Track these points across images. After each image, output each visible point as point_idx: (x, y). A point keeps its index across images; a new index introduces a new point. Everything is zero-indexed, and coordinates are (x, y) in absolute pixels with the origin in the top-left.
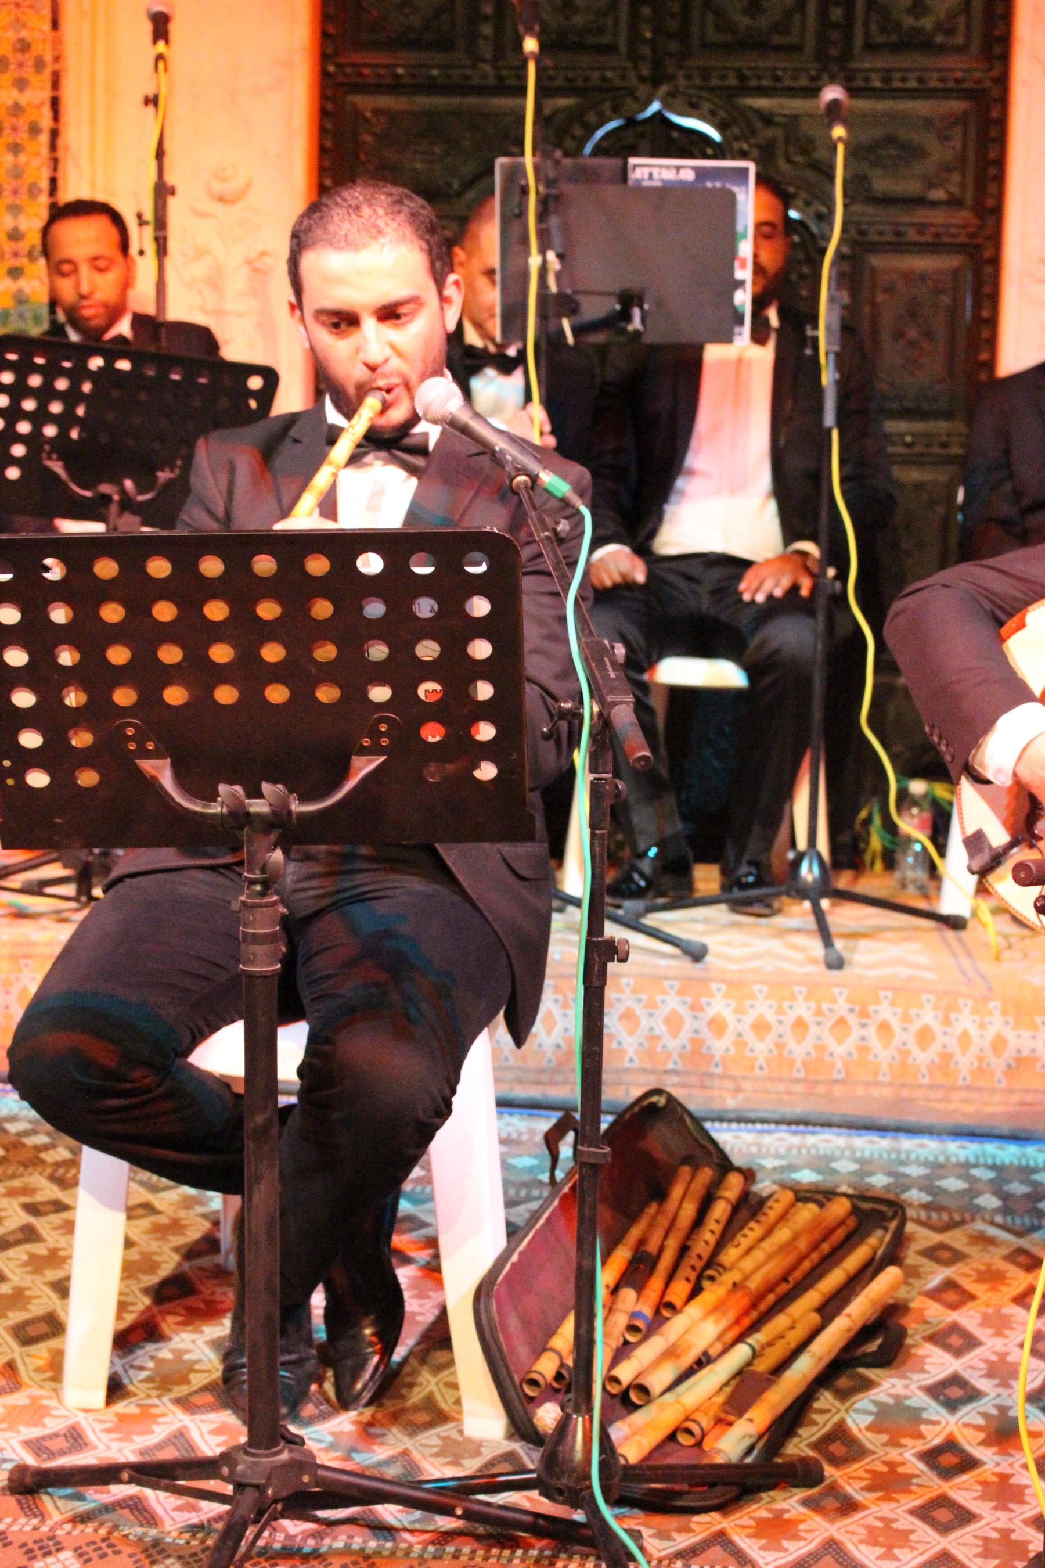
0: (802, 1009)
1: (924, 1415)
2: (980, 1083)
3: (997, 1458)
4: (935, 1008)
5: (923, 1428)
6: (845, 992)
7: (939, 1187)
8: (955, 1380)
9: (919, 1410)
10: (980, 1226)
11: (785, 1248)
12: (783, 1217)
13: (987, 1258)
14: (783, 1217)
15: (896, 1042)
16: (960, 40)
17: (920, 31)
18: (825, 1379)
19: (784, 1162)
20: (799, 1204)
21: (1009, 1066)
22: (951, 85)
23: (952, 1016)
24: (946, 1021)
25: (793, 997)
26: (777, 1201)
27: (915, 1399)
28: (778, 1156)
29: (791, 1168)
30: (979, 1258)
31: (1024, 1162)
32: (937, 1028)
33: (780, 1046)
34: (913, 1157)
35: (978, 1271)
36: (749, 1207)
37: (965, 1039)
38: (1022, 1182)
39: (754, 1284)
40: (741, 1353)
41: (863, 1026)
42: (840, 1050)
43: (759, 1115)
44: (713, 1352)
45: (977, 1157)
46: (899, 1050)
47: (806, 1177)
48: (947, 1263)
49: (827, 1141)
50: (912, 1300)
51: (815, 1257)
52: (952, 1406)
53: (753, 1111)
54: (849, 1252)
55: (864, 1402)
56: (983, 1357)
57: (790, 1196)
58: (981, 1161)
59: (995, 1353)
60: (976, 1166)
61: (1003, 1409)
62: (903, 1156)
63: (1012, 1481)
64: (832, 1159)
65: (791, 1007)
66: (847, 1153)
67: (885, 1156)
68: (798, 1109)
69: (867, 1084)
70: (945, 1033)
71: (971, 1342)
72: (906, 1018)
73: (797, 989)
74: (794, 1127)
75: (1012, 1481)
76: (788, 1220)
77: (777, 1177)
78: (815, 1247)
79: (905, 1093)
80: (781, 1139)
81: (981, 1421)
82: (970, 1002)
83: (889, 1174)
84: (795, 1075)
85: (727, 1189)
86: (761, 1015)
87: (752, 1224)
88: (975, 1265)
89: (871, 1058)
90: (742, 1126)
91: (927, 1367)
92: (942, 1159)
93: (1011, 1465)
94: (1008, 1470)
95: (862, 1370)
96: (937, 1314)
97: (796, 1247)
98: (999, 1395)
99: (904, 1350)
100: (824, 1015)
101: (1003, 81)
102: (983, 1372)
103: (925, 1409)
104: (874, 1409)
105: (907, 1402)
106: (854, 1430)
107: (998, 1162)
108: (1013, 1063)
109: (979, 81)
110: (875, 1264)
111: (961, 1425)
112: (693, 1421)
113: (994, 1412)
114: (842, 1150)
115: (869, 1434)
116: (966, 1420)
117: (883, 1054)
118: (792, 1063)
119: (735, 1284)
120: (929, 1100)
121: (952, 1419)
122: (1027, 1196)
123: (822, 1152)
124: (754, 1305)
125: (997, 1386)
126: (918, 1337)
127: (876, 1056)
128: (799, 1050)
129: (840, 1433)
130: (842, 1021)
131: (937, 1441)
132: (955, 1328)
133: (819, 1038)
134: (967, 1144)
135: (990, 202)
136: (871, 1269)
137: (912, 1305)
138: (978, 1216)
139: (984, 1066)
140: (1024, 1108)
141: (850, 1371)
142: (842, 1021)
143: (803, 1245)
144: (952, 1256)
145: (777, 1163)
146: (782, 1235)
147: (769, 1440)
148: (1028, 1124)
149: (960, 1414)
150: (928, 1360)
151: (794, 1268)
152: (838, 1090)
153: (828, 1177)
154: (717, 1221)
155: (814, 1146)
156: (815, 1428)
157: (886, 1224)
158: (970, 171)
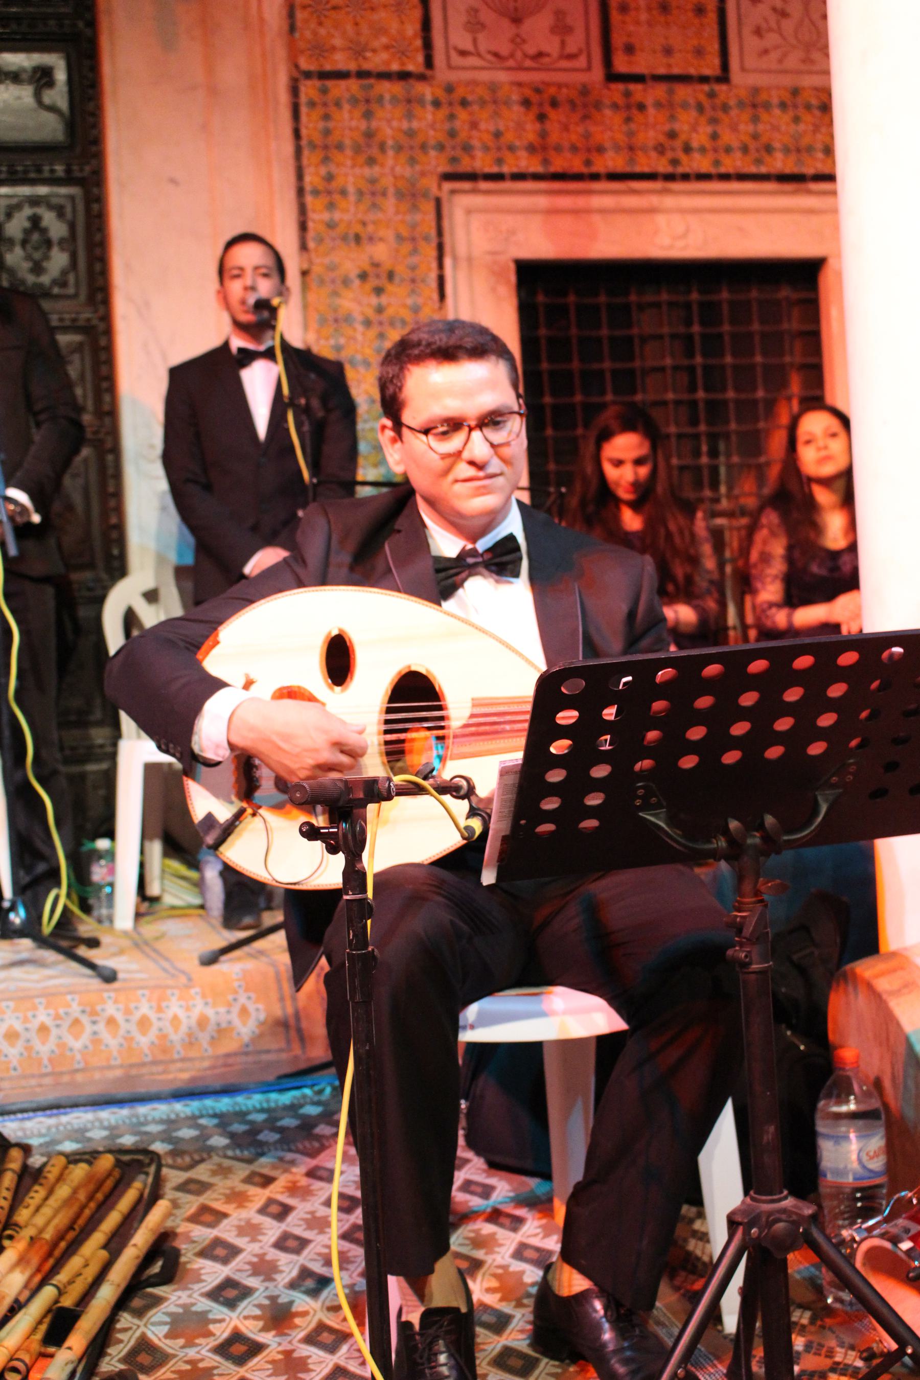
0: (43, 1016)
1: (211, 1316)
2: (193, 1054)
3: (277, 1339)
4: (149, 1001)
5: (211, 1327)
6: (77, 997)
7: (177, 1138)
8: (229, 1283)
9: (205, 1313)
10: (216, 1159)
11: (68, 1202)
12: (60, 1178)
13: (229, 1183)
14: (60, 1178)
15: (122, 1032)
16: (71, 290)
17: (41, 286)
18: (121, 1304)
19: (47, 1139)
20: (71, 1166)
21: (213, 1038)
22: (68, 323)
23: (164, 1004)
24: (160, 1009)
25: (35, 1008)
26: (53, 1166)
27: (199, 1304)
28: (41, 1135)
29: (54, 1142)
30: (222, 1185)
31: (237, 1109)
32: (153, 1016)
33: (29, 1049)
34: (150, 1118)
35: (224, 1194)
36: (29, 1177)
37: (175, 1020)
38: (240, 1123)
39: (48, 1235)
40: (48, 1293)
41: (94, 1023)
42: (77, 1045)
43: (19, 1106)
44: (22, 1299)
45: (200, 1111)
46: (125, 1038)
47: (69, 1146)
48: (198, 1193)
49: (78, 1118)
50: (178, 1226)
51: (92, 1205)
52: (231, 1304)
53: (13, 1104)
54: (120, 1196)
55: (157, 1315)
56: (246, 1260)
57: (63, 1160)
58: (204, 1112)
59: (255, 1255)
60: (201, 1116)
61: (273, 1299)
62: (142, 1119)
63: (295, 1355)
64: (86, 1130)
65: (34, 1016)
66: (97, 1124)
67: (127, 1121)
68: (51, 1096)
69: (102, 1069)
70: (159, 1019)
71: (234, 1251)
72: (128, 1012)
73: (37, 1001)
74: (48, 1112)
75: (295, 1355)
76: (64, 1180)
77: (43, 1150)
78: (91, 1198)
79: (134, 1072)
80: (41, 1123)
81: (258, 1312)
82: (176, 992)
83: (135, 1134)
84: (44, 1070)
85: (11, 1162)
86: (11, 1026)
87: (37, 1187)
88: (222, 1191)
89: (103, 1048)
90: (6, 1117)
91: (203, 1277)
92: (173, 1116)
93: (290, 1342)
94: (289, 1347)
95: (150, 1290)
96: (202, 1234)
97: (77, 1199)
98: (267, 1288)
99: (180, 1267)
100: (61, 1018)
101: (107, 319)
102: (250, 1272)
103: (210, 1311)
104: (168, 1319)
105: (194, 1309)
106: (155, 1340)
107: (218, 1111)
108: (215, 1035)
109: (88, 320)
110: (144, 1202)
111: (243, 1318)
112: (18, 1359)
113: (267, 1302)
114: (92, 1122)
115: (168, 1342)
116: (246, 1313)
117: (112, 1042)
118: (40, 1062)
119: (32, 1238)
120: (153, 1074)
121: (234, 1315)
122: (246, 1133)
123: (76, 1126)
124: (50, 1254)
125: (264, 1281)
126: (190, 1255)
127: (107, 1046)
128: (44, 1049)
129: (144, 1345)
130: (77, 1022)
131: (226, 1335)
132: (218, 1242)
133: (60, 1038)
134: (189, 1102)
135: (106, 408)
136: (141, 1208)
137: (179, 1230)
138: (213, 1154)
139: (193, 1040)
140: (228, 1069)
141: (140, 1293)
142: (77, 1022)
143: (82, 1196)
144: (200, 1187)
145: (42, 1140)
146: (63, 1191)
147: (87, 1363)
148: (232, 1080)
149: (239, 1309)
150: (203, 1271)
151: (74, 1221)
152: (79, 1077)
153: (87, 1144)
154: (8, 1189)
155: (68, 1123)
156: (122, 1345)
157: (146, 1169)
158: (89, 386)
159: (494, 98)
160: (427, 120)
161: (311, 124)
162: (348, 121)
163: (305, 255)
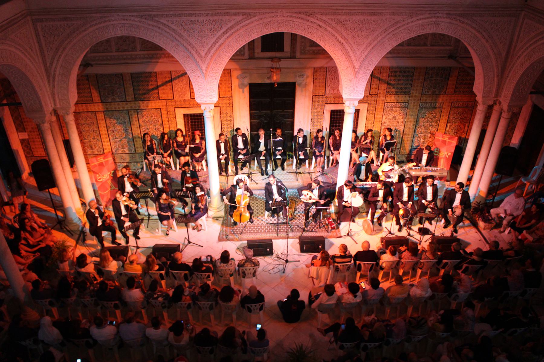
111: (299, 214)
159: (331, 97)
160: (324, 99)
161: (314, 100)
162: (317, 99)
163: (336, 273)
